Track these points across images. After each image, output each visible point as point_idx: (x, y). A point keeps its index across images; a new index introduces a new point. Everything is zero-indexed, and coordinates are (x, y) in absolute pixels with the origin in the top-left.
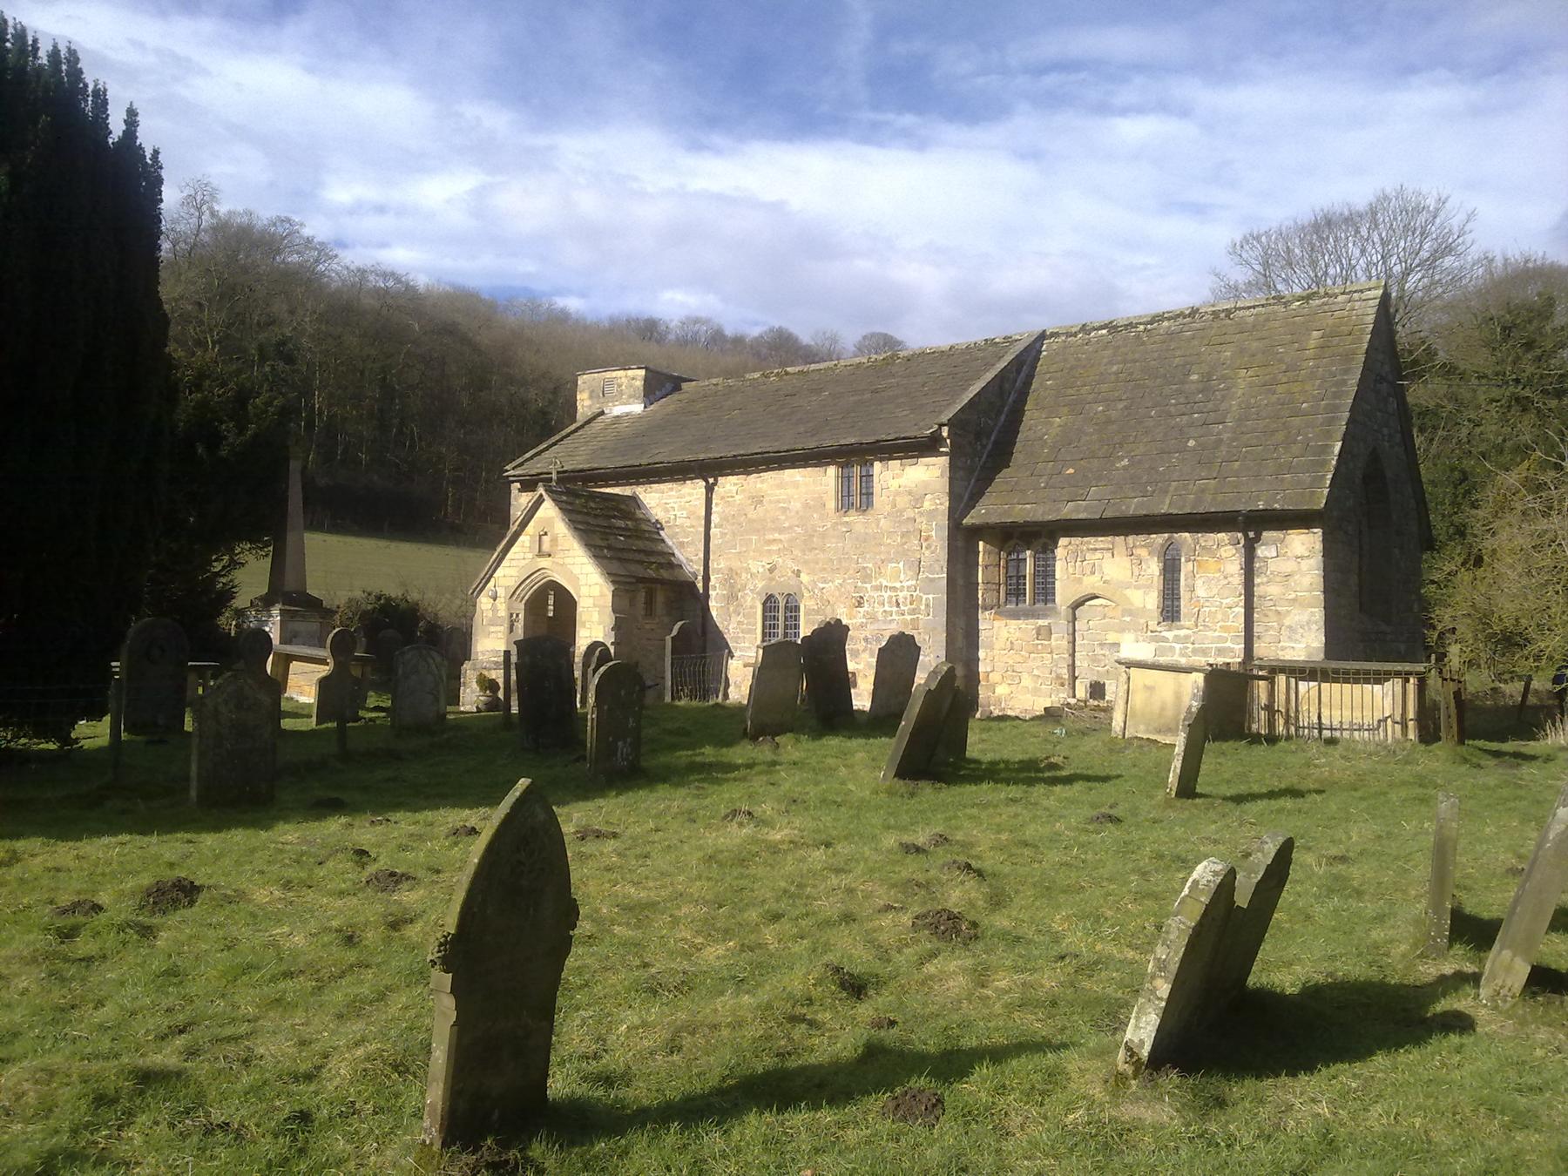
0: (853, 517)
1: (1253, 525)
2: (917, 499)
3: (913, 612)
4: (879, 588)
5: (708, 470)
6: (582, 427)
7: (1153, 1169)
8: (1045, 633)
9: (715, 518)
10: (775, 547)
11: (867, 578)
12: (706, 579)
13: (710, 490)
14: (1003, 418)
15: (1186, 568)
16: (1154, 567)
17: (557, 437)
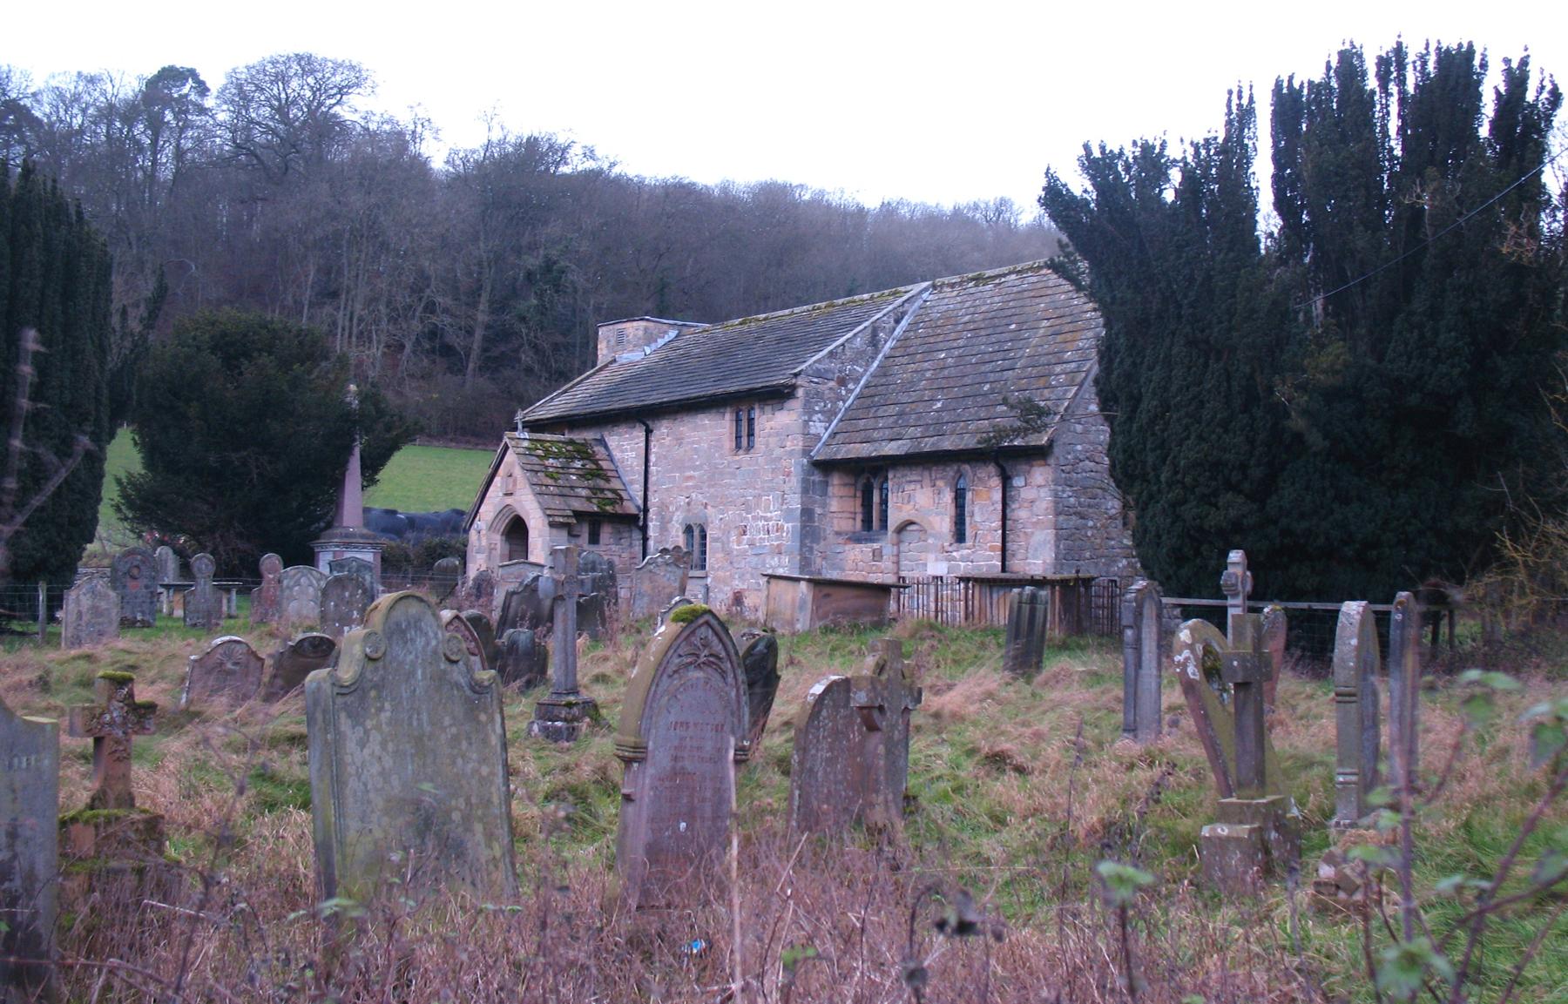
0: (742, 457)
1: (1005, 459)
3: (778, 538)
6: (601, 369)
7: (120, 1001)
9: (653, 458)
13: (649, 432)
14: (875, 364)
15: (969, 495)
16: (948, 497)
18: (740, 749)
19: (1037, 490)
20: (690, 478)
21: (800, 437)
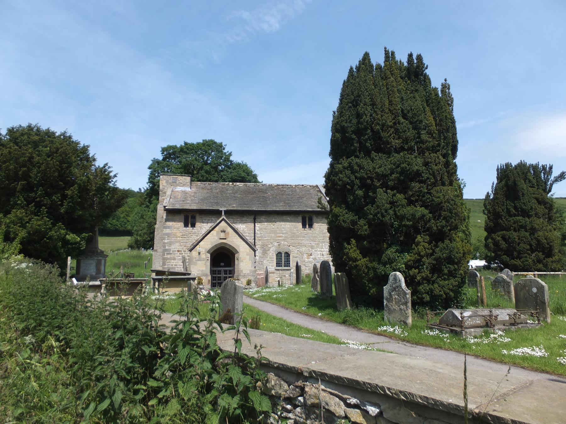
4: (316, 251)
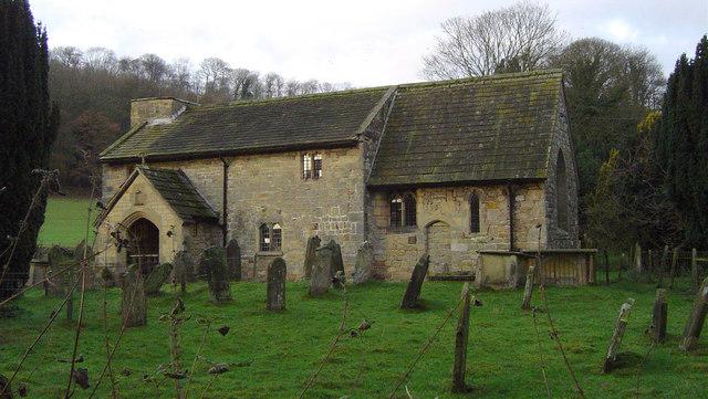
1: (514, 187)
2: (351, 167)
5: (226, 157)
8: (413, 240)
9: (229, 183)
10: (265, 198)
11: (319, 213)
12: (225, 215)
13: (226, 167)
15: (482, 206)
16: (467, 206)
17: (123, 138)
18: (588, 369)
19: (534, 205)
20: (264, 195)
21: (362, 173)
